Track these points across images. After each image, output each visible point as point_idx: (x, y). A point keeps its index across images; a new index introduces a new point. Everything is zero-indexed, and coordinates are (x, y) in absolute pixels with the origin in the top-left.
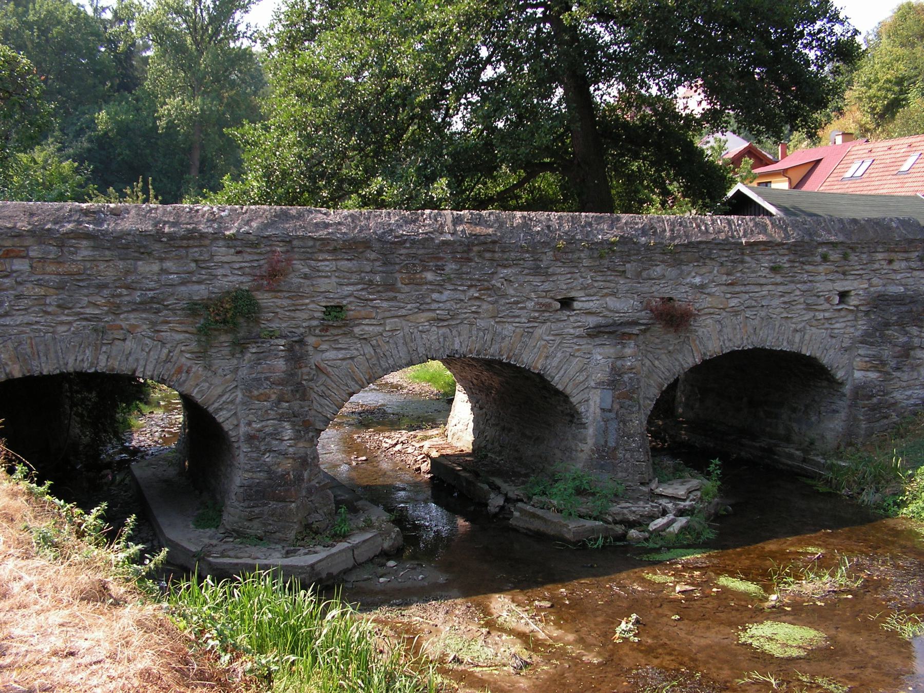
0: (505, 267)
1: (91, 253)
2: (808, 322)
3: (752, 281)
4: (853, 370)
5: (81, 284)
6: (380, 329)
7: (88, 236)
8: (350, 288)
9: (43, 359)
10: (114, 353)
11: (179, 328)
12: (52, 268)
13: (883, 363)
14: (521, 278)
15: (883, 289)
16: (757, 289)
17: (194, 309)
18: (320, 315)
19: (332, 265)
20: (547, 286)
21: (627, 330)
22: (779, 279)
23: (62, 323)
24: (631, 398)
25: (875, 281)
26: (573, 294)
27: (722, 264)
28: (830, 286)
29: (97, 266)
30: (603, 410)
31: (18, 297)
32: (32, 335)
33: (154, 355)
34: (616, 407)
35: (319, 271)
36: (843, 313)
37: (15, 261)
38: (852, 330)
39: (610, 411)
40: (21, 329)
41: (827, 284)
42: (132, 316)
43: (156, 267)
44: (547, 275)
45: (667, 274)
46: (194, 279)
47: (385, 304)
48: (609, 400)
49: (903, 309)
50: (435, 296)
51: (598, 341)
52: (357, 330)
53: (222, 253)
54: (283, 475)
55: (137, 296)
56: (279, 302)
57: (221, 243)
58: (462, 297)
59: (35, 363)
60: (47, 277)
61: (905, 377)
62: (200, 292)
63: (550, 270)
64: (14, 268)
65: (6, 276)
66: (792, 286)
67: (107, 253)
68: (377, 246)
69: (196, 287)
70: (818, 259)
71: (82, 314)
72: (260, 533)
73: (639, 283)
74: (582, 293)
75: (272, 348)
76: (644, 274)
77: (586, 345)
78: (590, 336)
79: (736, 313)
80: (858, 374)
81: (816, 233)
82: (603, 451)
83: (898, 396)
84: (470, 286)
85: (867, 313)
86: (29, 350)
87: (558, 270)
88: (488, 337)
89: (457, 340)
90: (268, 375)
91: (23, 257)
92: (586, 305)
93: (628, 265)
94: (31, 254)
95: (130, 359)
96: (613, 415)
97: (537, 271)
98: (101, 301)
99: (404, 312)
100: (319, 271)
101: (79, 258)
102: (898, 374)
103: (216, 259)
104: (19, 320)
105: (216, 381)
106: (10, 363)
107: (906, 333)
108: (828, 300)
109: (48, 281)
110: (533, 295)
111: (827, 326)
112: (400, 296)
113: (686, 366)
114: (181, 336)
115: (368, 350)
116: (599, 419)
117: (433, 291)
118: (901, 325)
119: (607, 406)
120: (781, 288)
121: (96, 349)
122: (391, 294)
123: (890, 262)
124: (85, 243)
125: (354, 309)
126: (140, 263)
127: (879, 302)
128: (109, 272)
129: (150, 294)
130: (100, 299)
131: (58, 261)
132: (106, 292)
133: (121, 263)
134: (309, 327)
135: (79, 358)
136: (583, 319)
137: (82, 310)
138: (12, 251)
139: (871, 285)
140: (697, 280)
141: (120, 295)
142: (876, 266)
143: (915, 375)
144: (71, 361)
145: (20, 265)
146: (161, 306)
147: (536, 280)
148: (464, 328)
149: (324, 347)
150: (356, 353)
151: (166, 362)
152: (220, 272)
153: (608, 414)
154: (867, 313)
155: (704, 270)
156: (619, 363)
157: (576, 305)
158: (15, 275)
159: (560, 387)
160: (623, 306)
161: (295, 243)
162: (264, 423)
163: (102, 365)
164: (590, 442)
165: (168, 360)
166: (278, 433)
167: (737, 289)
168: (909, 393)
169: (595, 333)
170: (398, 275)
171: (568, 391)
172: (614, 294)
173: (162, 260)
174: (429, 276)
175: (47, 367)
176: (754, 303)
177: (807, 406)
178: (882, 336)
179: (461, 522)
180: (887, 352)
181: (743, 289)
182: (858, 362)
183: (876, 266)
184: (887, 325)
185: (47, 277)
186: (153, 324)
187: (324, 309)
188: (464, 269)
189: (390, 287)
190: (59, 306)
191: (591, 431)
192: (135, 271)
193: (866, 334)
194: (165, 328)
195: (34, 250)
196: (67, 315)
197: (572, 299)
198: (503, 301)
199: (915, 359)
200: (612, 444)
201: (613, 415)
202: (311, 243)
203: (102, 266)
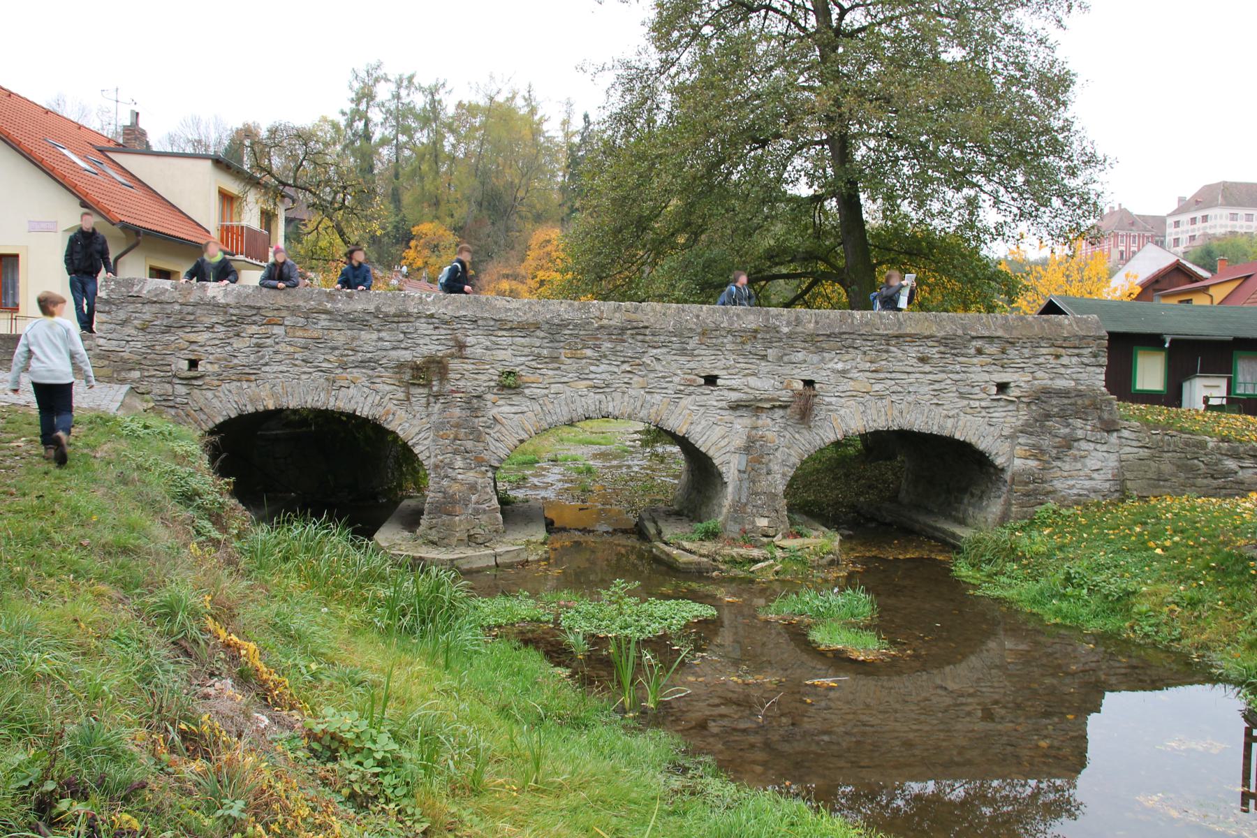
0: (655, 348)
2: (961, 409)
3: (897, 369)
4: (1011, 457)
6: (546, 391)
7: (326, 312)
8: (523, 359)
11: (389, 381)
12: (299, 333)
13: (1042, 452)
14: (669, 358)
15: (1050, 382)
16: (905, 376)
17: (400, 366)
19: (509, 340)
20: (692, 365)
21: (760, 405)
22: (927, 368)
24: (760, 463)
25: (1039, 374)
26: (715, 373)
27: (865, 353)
28: (986, 377)
31: (276, 352)
33: (370, 400)
36: (1002, 403)
38: (1014, 420)
41: (983, 375)
43: (375, 336)
44: (692, 355)
45: (808, 359)
47: (551, 373)
49: (1066, 401)
50: (592, 368)
51: (738, 413)
52: (527, 391)
53: (423, 327)
55: (359, 357)
56: (466, 366)
57: (423, 320)
58: (616, 370)
61: (1067, 467)
62: (406, 356)
63: (696, 352)
66: (943, 376)
68: (546, 327)
69: (404, 352)
70: (972, 351)
72: (435, 539)
74: (724, 372)
76: (786, 359)
77: (728, 416)
78: (731, 408)
79: (881, 397)
80: (1018, 462)
81: (972, 328)
83: (1058, 485)
84: (623, 362)
85: (1028, 404)
87: (703, 352)
88: (639, 404)
89: (611, 404)
92: (728, 382)
93: (770, 351)
96: (746, 476)
97: (683, 352)
98: (332, 358)
99: (565, 379)
102: (1059, 463)
104: (276, 368)
105: (415, 422)
107: (1068, 425)
108: (984, 390)
110: (679, 372)
111: (984, 414)
112: (563, 367)
113: (827, 441)
114: (388, 388)
115: (537, 408)
117: (592, 364)
118: (1063, 416)
120: (930, 377)
122: (556, 365)
123: (1058, 357)
124: (324, 316)
125: (527, 376)
127: (1040, 396)
128: (340, 338)
129: (369, 355)
131: (303, 328)
132: (337, 353)
134: (489, 387)
136: (726, 393)
139: (1035, 379)
140: (840, 366)
142: (1041, 360)
143: (1079, 466)
144: (310, 401)
145: (277, 330)
147: (683, 359)
148: (617, 395)
149: (500, 403)
150: (526, 409)
152: (421, 342)
154: (1028, 404)
155: (847, 357)
156: (754, 432)
157: (719, 382)
159: (703, 449)
160: (763, 384)
161: (480, 322)
163: (332, 405)
164: (730, 498)
165: (379, 405)
167: (882, 375)
168: (1071, 483)
169: (735, 407)
170: (562, 351)
171: (710, 453)
172: (754, 374)
173: (379, 331)
174: (589, 352)
175: (293, 404)
176: (900, 389)
177: (983, 492)
178: (1042, 426)
180: (1046, 442)
181: (888, 375)
182: (1019, 450)
183: (1041, 360)
184: (1048, 416)
186: (370, 377)
188: (618, 348)
189: (555, 359)
192: (359, 338)
193: (1026, 424)
194: (378, 380)
197: (716, 377)
198: (652, 375)
199: (1079, 450)
200: (744, 500)
201: (746, 476)
202: (492, 323)
203: (335, 333)
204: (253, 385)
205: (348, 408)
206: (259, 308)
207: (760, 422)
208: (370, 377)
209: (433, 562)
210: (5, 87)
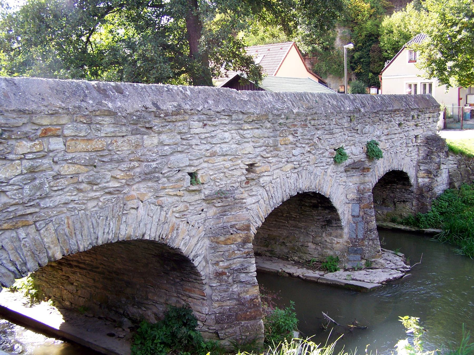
1: (113, 130)
3: (393, 132)
5: (104, 160)
7: (111, 113)
9: (79, 237)
10: (130, 221)
12: (82, 145)
18: (245, 172)
23: (92, 199)
29: (116, 141)
30: (353, 216)
31: (56, 177)
32: (68, 214)
34: (362, 214)
35: (245, 138)
37: (51, 139)
39: (358, 216)
40: (59, 210)
42: (141, 185)
46: (179, 149)
48: (357, 209)
54: (252, 300)
59: (73, 241)
60: (78, 155)
64: (51, 147)
65: (44, 157)
67: (124, 129)
70: (411, 118)
71: (107, 188)
73: (362, 136)
75: (237, 201)
82: (356, 241)
86: (67, 230)
90: (233, 223)
91: (58, 136)
94: (67, 132)
95: (141, 225)
98: (120, 174)
100: (245, 138)
101: (103, 135)
103: (192, 131)
106: (52, 246)
109: (79, 159)
116: (352, 222)
119: (356, 214)
121: (119, 221)
124: (107, 119)
126: (145, 137)
129: (154, 165)
130: (119, 172)
132: (124, 166)
133: (133, 137)
135: (106, 231)
137: (106, 185)
138: (51, 130)
141: (134, 167)
145: (56, 144)
146: (161, 175)
151: (164, 223)
153: (357, 219)
158: (51, 154)
162: (231, 262)
164: (346, 237)
166: (246, 268)
173: (159, 133)
179: (417, 318)
185: (78, 155)
186: (156, 191)
187: (247, 167)
190: (89, 183)
191: (346, 230)
195: (68, 128)
196: (96, 191)
201: (360, 219)
204: (32, 230)
205: (136, 235)
206: (32, 113)
207: (367, 179)
208: (156, 191)
209: (402, 223)
210: (469, 131)
